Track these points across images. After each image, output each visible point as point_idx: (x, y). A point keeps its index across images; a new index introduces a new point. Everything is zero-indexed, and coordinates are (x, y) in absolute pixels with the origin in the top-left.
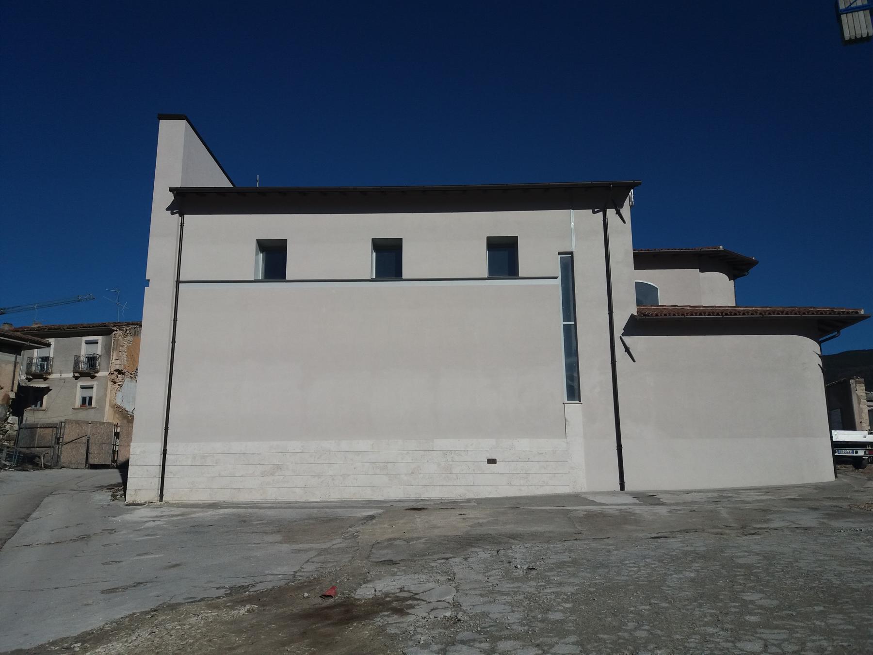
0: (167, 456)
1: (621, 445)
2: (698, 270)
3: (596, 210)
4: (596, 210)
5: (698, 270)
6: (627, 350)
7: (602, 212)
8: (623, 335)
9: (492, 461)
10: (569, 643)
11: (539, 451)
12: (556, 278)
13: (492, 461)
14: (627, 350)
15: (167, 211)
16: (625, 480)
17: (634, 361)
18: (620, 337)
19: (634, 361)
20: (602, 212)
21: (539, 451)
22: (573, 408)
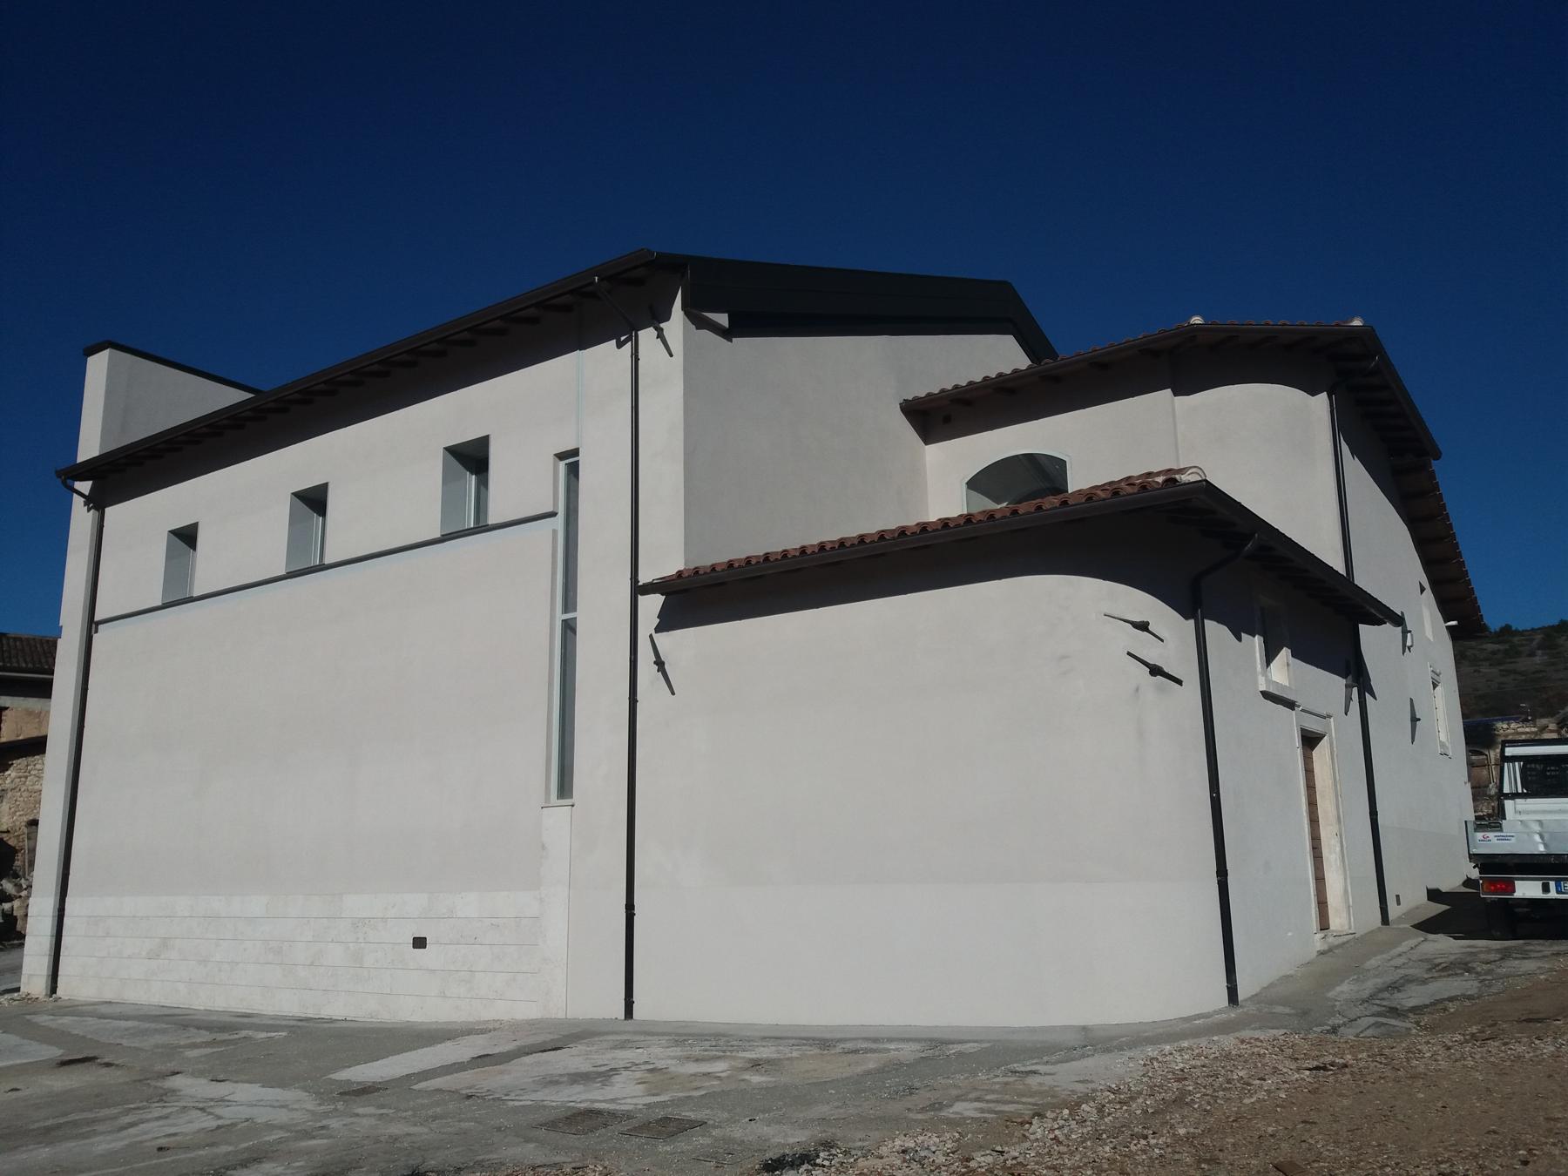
0: (66, 920)
1: (634, 906)
2: (1169, 391)
3: (623, 338)
4: (623, 338)
5: (1169, 391)
6: (660, 663)
7: (1360, 625)
8: (658, 629)
9: (419, 943)
10: (626, 1068)
11: (494, 921)
12: (553, 514)
13: (419, 943)
14: (660, 663)
15: (325, 482)
16: (636, 998)
17: (673, 693)
18: (651, 636)
19: (673, 693)
20: (1360, 625)
21: (494, 921)
22: (558, 818)
